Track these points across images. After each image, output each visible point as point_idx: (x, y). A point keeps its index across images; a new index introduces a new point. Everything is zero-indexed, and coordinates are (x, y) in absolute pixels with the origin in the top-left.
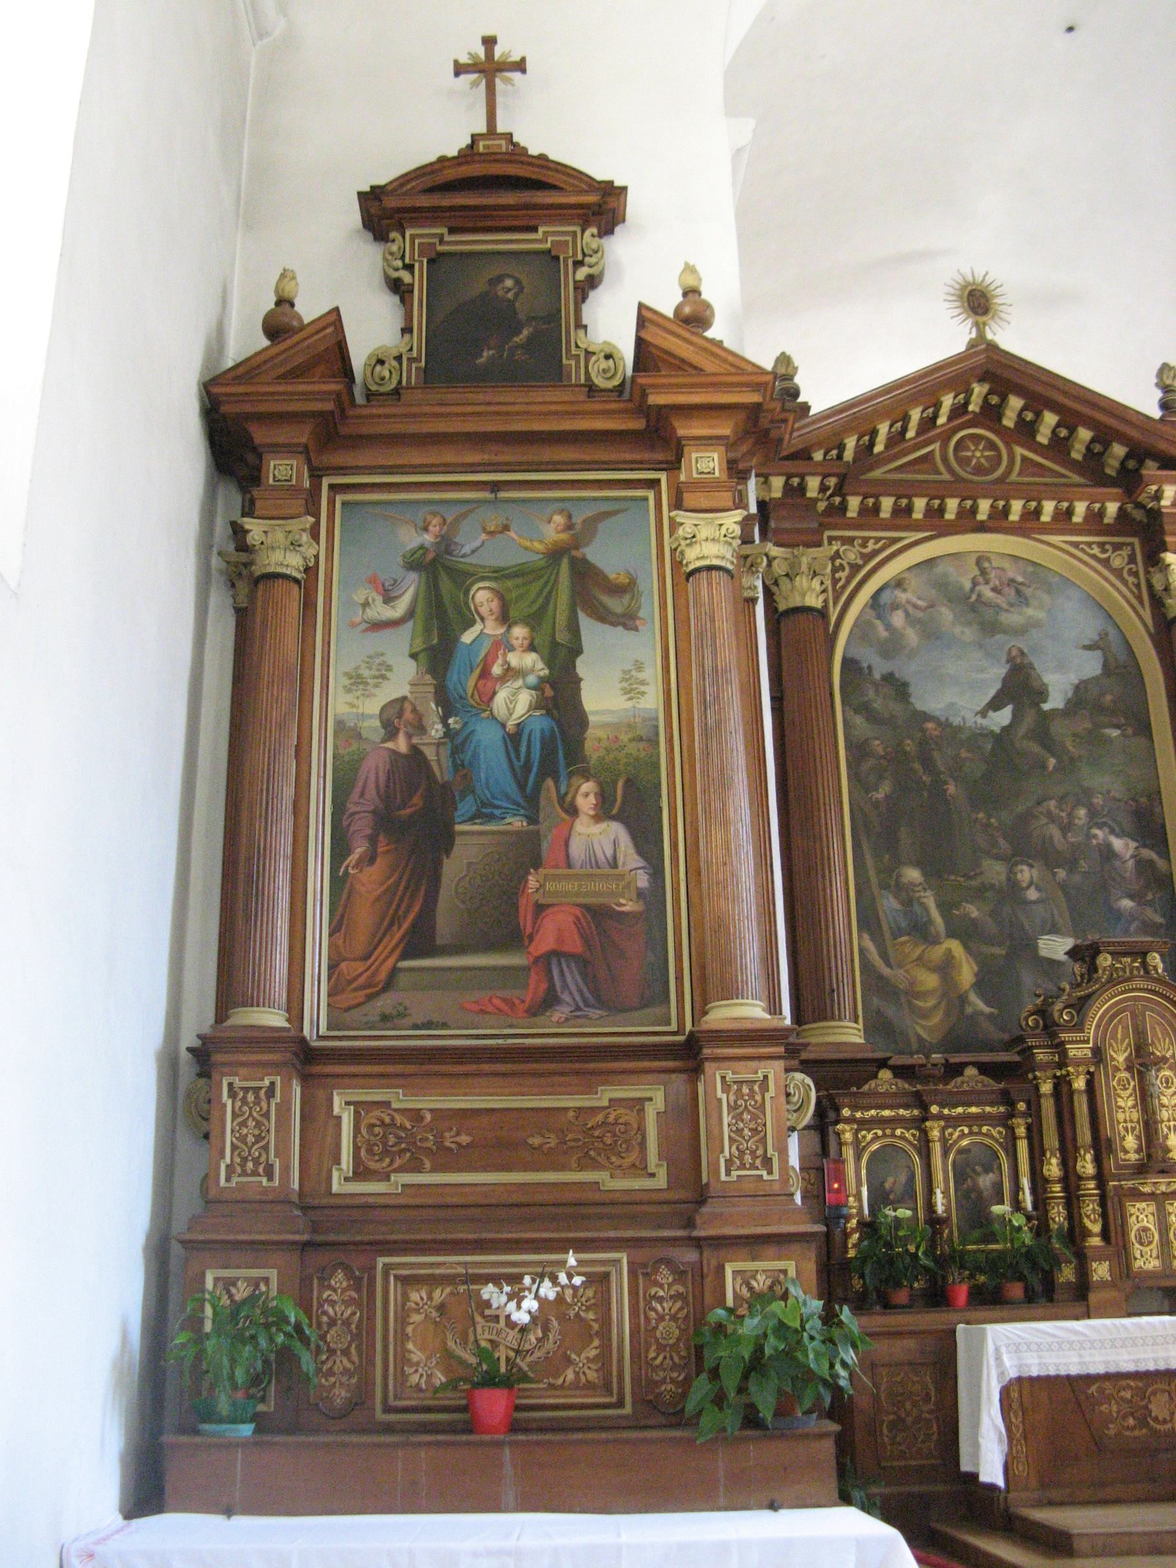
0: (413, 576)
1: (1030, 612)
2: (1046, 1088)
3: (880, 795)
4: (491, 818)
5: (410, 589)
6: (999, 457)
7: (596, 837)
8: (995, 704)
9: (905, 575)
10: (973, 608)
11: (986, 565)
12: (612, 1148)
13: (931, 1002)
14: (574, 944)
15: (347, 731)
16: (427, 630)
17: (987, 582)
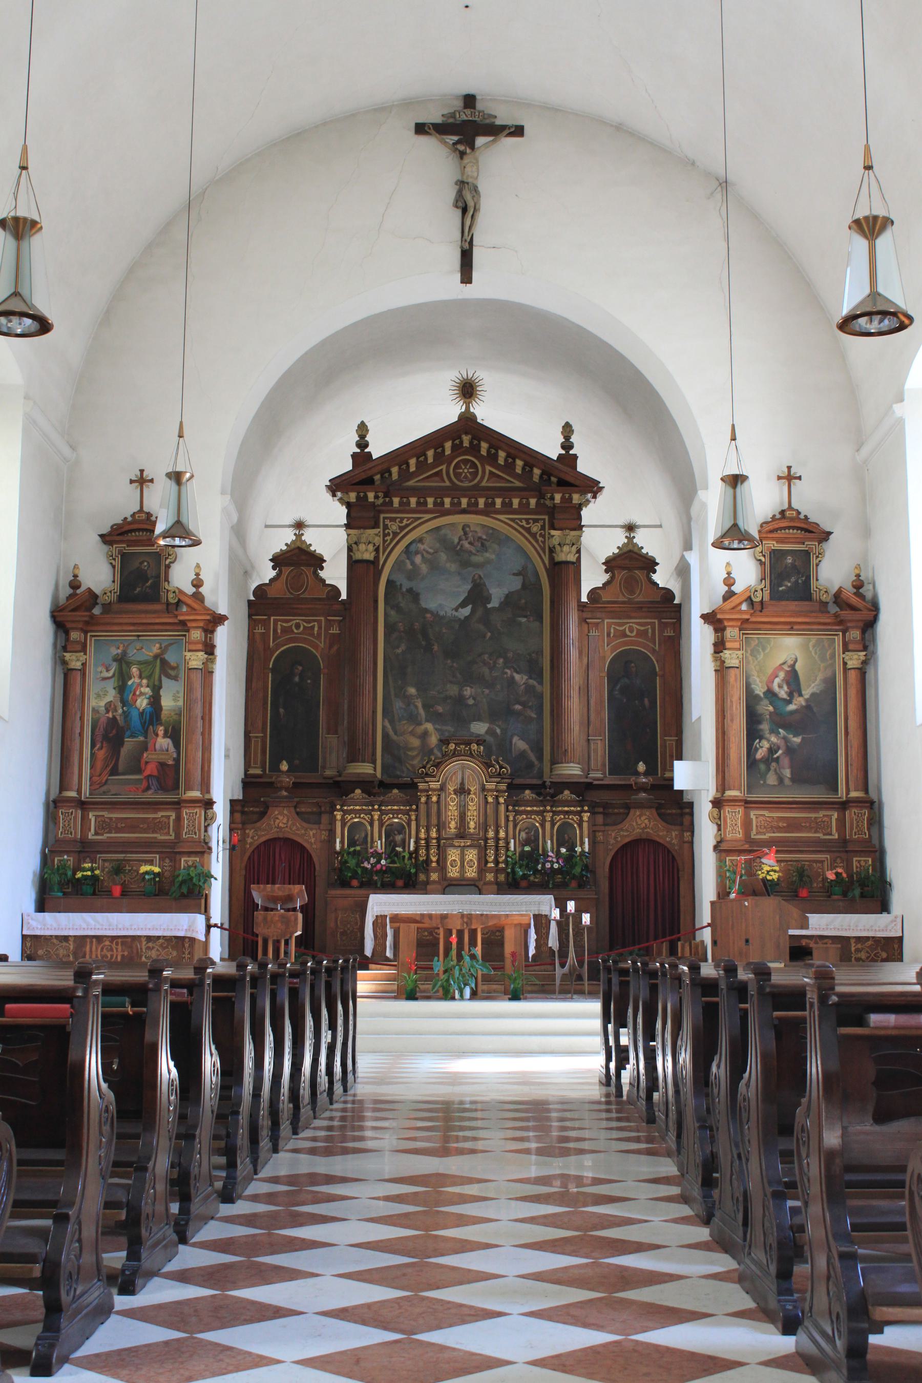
0: (115, 664)
1: (487, 555)
2: (423, 799)
3: (399, 651)
4: (135, 737)
5: (114, 667)
7: (163, 742)
8: (463, 605)
10: (458, 553)
11: (467, 529)
12: (161, 828)
13: (415, 753)
14: (155, 773)
15: (95, 711)
16: (118, 681)
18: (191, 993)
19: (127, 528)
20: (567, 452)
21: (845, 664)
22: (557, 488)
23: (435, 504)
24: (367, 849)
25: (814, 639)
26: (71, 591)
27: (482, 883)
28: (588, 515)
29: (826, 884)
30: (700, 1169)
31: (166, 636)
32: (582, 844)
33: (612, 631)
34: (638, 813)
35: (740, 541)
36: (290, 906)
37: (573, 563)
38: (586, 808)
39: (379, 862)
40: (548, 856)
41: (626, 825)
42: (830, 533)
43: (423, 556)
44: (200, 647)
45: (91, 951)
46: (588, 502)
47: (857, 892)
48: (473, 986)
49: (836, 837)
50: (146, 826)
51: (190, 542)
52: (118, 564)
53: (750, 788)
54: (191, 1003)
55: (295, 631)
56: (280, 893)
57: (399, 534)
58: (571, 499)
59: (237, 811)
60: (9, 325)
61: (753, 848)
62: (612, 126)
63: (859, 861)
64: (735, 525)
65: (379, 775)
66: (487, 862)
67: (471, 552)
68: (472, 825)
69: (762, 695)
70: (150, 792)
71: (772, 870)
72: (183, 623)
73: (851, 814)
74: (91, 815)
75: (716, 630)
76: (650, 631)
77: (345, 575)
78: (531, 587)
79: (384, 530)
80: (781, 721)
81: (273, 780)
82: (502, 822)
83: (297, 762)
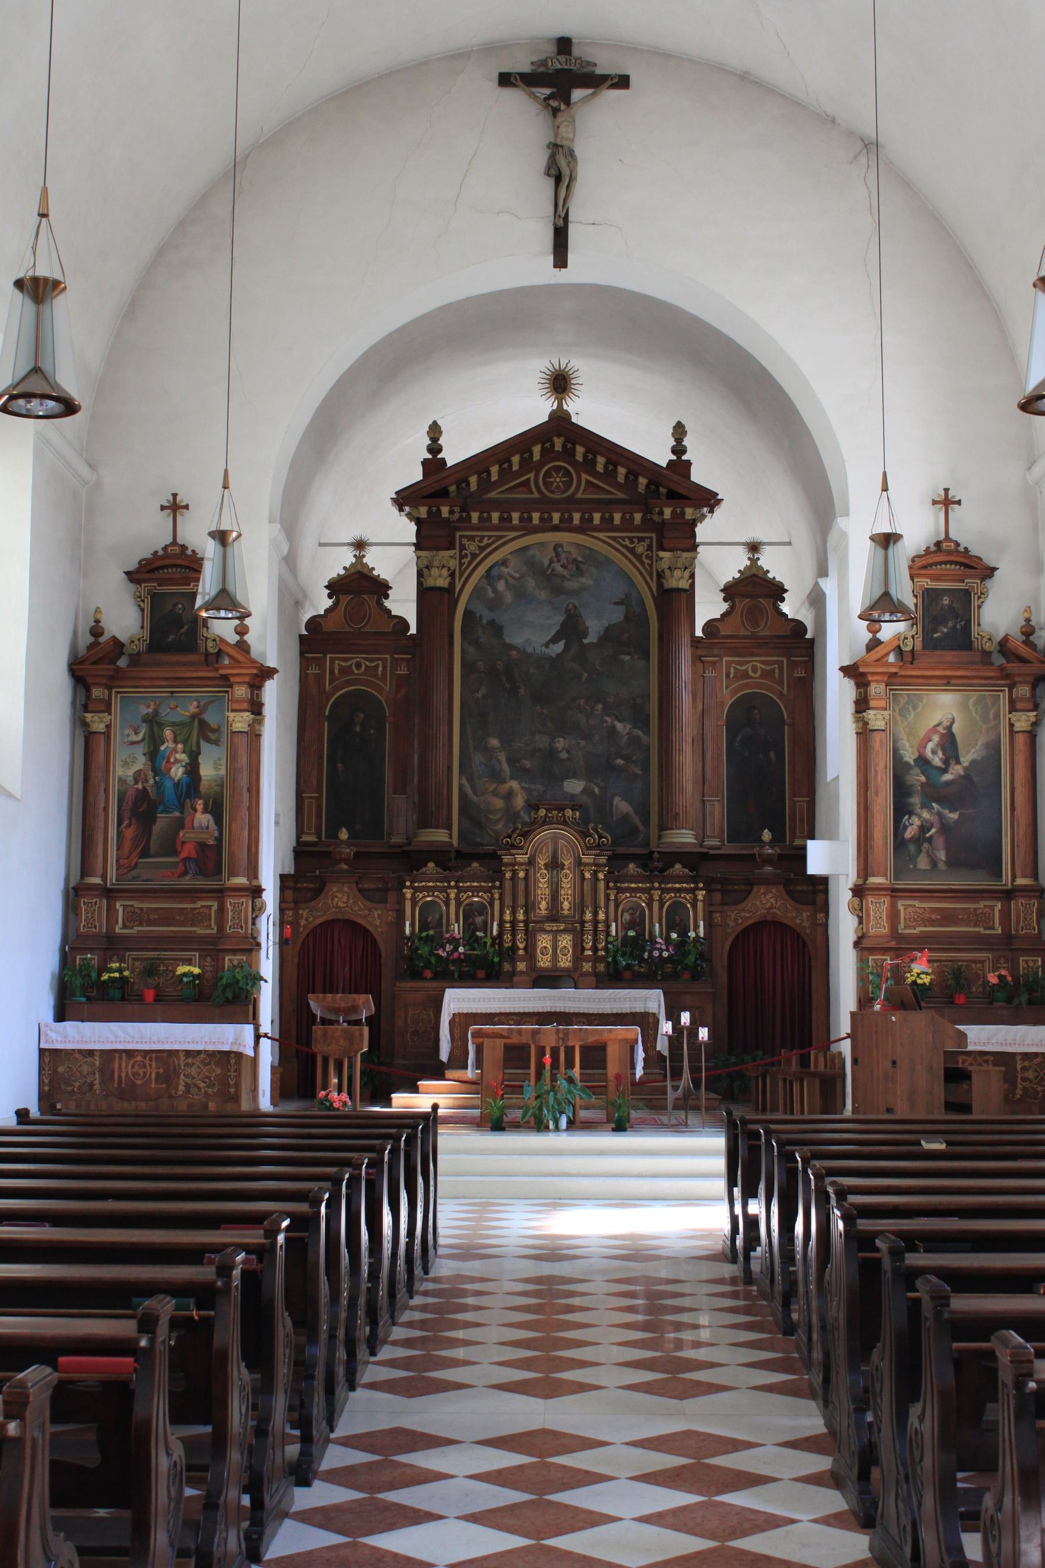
1: (583, 580)
2: (508, 875)
3: (479, 695)
6: (571, 482)
7: (202, 819)
8: (555, 640)
9: (509, 557)
11: (560, 549)
13: (498, 816)
14: (194, 855)
15: (122, 781)
16: (149, 746)
17: (559, 561)
18: (260, 1260)
19: (157, 564)
20: (679, 458)
21: (1011, 725)
22: (666, 500)
23: (521, 519)
24: (442, 932)
25: (974, 696)
26: (92, 639)
27: (577, 974)
28: (702, 531)
29: (988, 989)
30: (856, 1458)
31: (204, 693)
32: (696, 927)
33: (732, 671)
34: (762, 890)
35: (892, 614)
36: (353, 1017)
37: (686, 591)
38: (701, 885)
39: (456, 949)
40: (657, 943)
41: (748, 904)
42: (995, 569)
43: (507, 582)
44: (245, 706)
45: (120, 1068)
46: (704, 517)
47: (1024, 998)
48: (571, 1115)
49: (1000, 931)
50: (182, 918)
51: (238, 615)
52: (147, 606)
53: (897, 874)
54: (261, 1272)
55: (356, 671)
56: (343, 1005)
57: (478, 555)
58: (683, 513)
59: (289, 888)
60: (28, 406)
61: (902, 946)
62: (736, 75)
63: (1027, 962)
64: (886, 594)
65: (455, 842)
66: (583, 949)
67: (564, 577)
68: (566, 905)
69: (912, 763)
70: (188, 877)
71: (923, 973)
72: (225, 678)
73: (1017, 905)
74: (118, 905)
75: (858, 685)
76: (777, 671)
77: (415, 597)
78: (635, 617)
79: (461, 551)
80: (935, 794)
81: (331, 849)
82: (602, 902)
83: (358, 827)
